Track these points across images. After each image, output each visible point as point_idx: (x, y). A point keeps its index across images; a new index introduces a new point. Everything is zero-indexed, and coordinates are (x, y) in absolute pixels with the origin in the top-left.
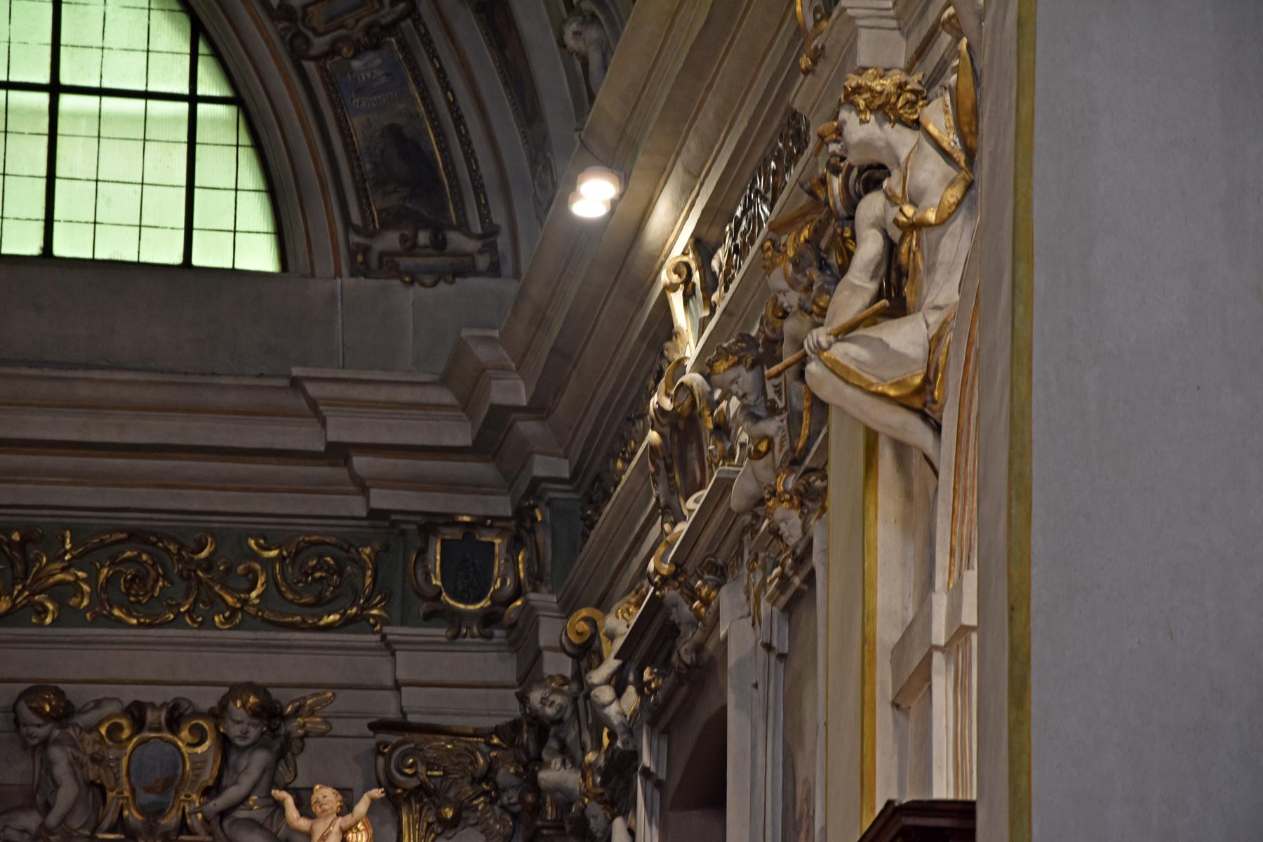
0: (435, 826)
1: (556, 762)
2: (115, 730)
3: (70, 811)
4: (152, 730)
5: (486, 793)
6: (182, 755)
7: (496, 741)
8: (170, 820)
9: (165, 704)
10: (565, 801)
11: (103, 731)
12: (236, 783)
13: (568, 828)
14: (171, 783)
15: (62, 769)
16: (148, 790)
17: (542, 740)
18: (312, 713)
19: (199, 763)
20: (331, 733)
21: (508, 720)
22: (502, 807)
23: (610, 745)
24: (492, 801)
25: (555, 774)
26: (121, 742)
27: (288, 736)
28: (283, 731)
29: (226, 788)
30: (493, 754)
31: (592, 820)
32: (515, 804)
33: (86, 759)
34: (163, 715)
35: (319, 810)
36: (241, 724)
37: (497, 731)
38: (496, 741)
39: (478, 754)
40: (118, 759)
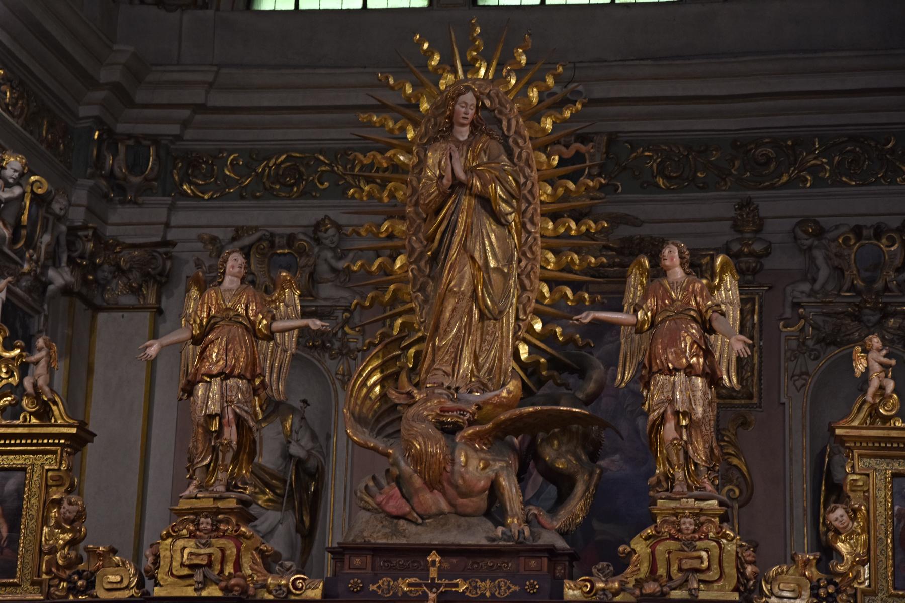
8: (879, 285)
9: (872, 226)
11: (840, 241)
19: (893, 255)
34: (872, 231)
40: (849, 255)
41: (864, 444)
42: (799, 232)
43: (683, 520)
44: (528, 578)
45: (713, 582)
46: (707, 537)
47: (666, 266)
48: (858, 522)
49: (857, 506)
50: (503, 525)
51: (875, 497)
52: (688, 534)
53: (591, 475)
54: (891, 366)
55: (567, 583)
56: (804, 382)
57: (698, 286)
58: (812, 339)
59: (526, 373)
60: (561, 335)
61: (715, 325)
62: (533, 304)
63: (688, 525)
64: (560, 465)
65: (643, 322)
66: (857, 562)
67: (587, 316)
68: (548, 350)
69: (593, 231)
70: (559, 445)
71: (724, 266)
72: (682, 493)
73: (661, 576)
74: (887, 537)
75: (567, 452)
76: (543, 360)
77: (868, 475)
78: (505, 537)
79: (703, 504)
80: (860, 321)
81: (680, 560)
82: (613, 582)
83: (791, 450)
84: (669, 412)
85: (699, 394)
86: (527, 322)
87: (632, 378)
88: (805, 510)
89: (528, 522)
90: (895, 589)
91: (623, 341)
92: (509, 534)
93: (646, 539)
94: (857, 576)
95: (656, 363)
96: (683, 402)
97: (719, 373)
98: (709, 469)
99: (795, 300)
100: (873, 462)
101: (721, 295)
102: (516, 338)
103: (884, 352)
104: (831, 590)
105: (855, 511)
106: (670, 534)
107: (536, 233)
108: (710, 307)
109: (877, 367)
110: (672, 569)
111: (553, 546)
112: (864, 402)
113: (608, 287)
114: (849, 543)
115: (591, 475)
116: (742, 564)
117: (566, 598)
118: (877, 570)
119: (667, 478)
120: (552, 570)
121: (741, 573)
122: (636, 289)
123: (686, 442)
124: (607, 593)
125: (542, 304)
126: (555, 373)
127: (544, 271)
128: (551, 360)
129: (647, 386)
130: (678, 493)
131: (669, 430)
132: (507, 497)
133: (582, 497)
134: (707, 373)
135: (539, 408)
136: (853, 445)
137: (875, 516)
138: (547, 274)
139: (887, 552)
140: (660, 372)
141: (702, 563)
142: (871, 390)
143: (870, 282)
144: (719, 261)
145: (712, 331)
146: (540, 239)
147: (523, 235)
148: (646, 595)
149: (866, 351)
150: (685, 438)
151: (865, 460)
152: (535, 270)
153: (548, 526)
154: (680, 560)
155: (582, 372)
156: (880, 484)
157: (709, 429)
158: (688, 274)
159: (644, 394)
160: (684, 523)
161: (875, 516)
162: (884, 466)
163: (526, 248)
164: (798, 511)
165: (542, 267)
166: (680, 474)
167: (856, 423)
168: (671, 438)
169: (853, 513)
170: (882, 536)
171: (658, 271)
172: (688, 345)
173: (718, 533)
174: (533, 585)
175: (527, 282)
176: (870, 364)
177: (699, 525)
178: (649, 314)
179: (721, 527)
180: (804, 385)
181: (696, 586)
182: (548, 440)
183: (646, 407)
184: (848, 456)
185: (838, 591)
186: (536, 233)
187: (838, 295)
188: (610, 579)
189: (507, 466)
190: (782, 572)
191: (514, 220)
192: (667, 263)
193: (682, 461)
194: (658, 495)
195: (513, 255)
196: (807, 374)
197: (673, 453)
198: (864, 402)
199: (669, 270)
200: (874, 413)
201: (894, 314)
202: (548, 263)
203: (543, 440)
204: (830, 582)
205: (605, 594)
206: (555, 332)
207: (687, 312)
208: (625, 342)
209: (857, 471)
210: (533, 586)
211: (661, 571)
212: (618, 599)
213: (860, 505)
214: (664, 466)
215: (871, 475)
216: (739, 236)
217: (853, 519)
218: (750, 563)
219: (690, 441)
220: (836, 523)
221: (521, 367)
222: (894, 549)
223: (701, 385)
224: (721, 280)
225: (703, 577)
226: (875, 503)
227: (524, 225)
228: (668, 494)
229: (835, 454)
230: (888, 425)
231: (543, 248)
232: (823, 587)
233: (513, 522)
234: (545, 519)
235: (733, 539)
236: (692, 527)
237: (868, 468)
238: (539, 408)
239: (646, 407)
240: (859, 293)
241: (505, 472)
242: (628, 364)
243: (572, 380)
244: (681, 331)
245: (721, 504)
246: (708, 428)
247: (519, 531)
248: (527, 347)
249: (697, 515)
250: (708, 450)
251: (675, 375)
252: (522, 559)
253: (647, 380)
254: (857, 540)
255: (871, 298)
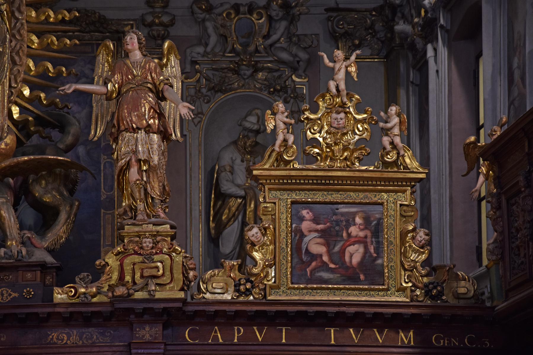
0: (352, 47)
1: (401, 22)
2: (229, 14)
3: (215, 46)
4: (242, 14)
5: (370, 34)
6: (254, 23)
7: (374, 13)
8: (252, 48)
9: (247, 4)
10: (404, 36)
11: (225, 15)
12: (275, 34)
13: (406, 47)
14: (251, 34)
15: (211, 30)
16: (243, 37)
17: (394, 14)
18: (302, 5)
19: (261, 26)
20: (310, 13)
21: (379, 5)
22: (377, 39)
23: (425, 15)
24: (373, 37)
25: (401, 27)
26: (231, 19)
27: (293, 14)
28: (291, 13)
29: (271, 36)
30: (373, 18)
31: (417, 45)
32: (383, 37)
33: (219, 26)
34: (246, 8)
35: (337, 59)
36: (276, 11)
37: (374, 9)
38: (374, 13)
39: (368, 19)
40: (231, 26)
41: (273, 181)
42: (195, 7)
43: (144, 240)
44: (26, 286)
45: (165, 285)
46: (161, 252)
47: (129, 50)
48: (268, 237)
49: (267, 225)
50: (4, 247)
51: (280, 219)
52: (148, 250)
53: (71, 206)
54: (291, 124)
55: (57, 290)
56: (200, 119)
57: (152, 65)
58: (205, 88)
59: (17, 128)
60: (45, 99)
61: (166, 94)
62: (22, 76)
63: (148, 244)
64: (47, 199)
65: (112, 92)
66: (267, 266)
67: (70, 88)
68: (35, 111)
69: (67, 19)
70: (46, 184)
71: (170, 48)
72: (144, 220)
73: (128, 282)
74: (287, 247)
75: (53, 189)
76: (30, 119)
77: (275, 203)
78: (7, 256)
79: (159, 228)
80: (238, 74)
81: (142, 269)
82: (92, 287)
83: (191, 169)
84: (133, 160)
85: (155, 146)
86: (17, 89)
87: (104, 134)
88: (200, 212)
89: (23, 243)
90: (292, 283)
91: (94, 105)
92: (10, 254)
93: (116, 255)
94: (266, 276)
95: (124, 124)
96: (144, 152)
97: (169, 130)
98: (162, 201)
99: (193, 59)
100: (278, 193)
101: (168, 71)
102: (10, 102)
103: (286, 114)
104: (248, 286)
105: (265, 229)
106: (134, 251)
107: (22, 19)
108: (162, 81)
109: (282, 126)
110: (136, 277)
111: (45, 262)
112: (273, 150)
113: (80, 63)
114: (261, 252)
115: (71, 206)
116: (186, 270)
117: (55, 301)
118: (280, 270)
119: (131, 209)
120: (43, 280)
121: (186, 277)
122: (103, 65)
123: (145, 182)
124: (87, 296)
125: (29, 75)
126: (41, 129)
127: (30, 50)
128: (37, 118)
129: (116, 140)
130: (141, 220)
131: (133, 174)
132: (7, 225)
133: (65, 223)
134: (161, 131)
135: (32, 157)
136: (265, 181)
137: (279, 232)
138: (32, 52)
139: (287, 258)
140: (127, 130)
141: (159, 271)
142: (278, 142)
143: (245, 46)
144: (166, 45)
145: (164, 99)
146: (25, 24)
147: (12, 20)
148: (117, 297)
149: (274, 114)
150: (145, 179)
151: (272, 192)
152: (23, 48)
153: (38, 246)
154: (142, 269)
155: (62, 126)
156: (283, 209)
157: (162, 172)
158: (145, 56)
159: (114, 146)
160: (145, 243)
161: (279, 232)
162: (286, 196)
163: (15, 32)
164: (196, 213)
165: (28, 47)
166: (141, 206)
167: (267, 166)
168: (134, 179)
169: (264, 231)
170: (284, 246)
171: (121, 53)
172: (147, 110)
173: (170, 249)
174: (29, 292)
175: (17, 58)
176: (277, 123)
177: (156, 243)
178: (117, 86)
179: (172, 244)
180: (199, 122)
181: (153, 288)
182: (37, 181)
183: (115, 156)
184: (261, 190)
185: (253, 287)
186: (22, 19)
187: (224, 56)
188: (89, 285)
189: (6, 202)
190: (215, 275)
191: (6, 10)
192: (129, 47)
193: (143, 196)
194: (125, 222)
195: (6, 37)
196: (202, 113)
197: (136, 190)
198: (273, 150)
199: (130, 52)
200: (280, 159)
201: (262, 69)
202: (33, 43)
203: (33, 181)
204: (248, 281)
205: (85, 297)
206: (40, 97)
207: (145, 85)
208: (96, 106)
209: (267, 200)
210: (29, 293)
211: (128, 278)
212: (95, 300)
213: (269, 225)
214: (129, 200)
215: (277, 203)
216: (151, 10)
217: (264, 235)
218: (192, 269)
219: (148, 182)
220: (253, 239)
221: (13, 124)
222: (292, 255)
223: (156, 140)
224: (168, 60)
225: (159, 281)
226: (279, 223)
227: (13, 13)
228: (132, 221)
229: (222, 172)
230: (288, 167)
231: (28, 31)
232: (243, 284)
233: (12, 244)
234: (36, 240)
235: (181, 252)
236: (151, 245)
237: (275, 198)
238: (32, 157)
239: (115, 156)
240: (238, 54)
241: (5, 207)
242: (99, 123)
243: (55, 134)
244: (141, 99)
245: (172, 227)
246: (162, 171)
247: (18, 252)
248: (18, 108)
249: (155, 236)
250: (161, 188)
251: (138, 133)
252: (20, 272)
253: (116, 136)
254: (267, 249)
255: (246, 58)
